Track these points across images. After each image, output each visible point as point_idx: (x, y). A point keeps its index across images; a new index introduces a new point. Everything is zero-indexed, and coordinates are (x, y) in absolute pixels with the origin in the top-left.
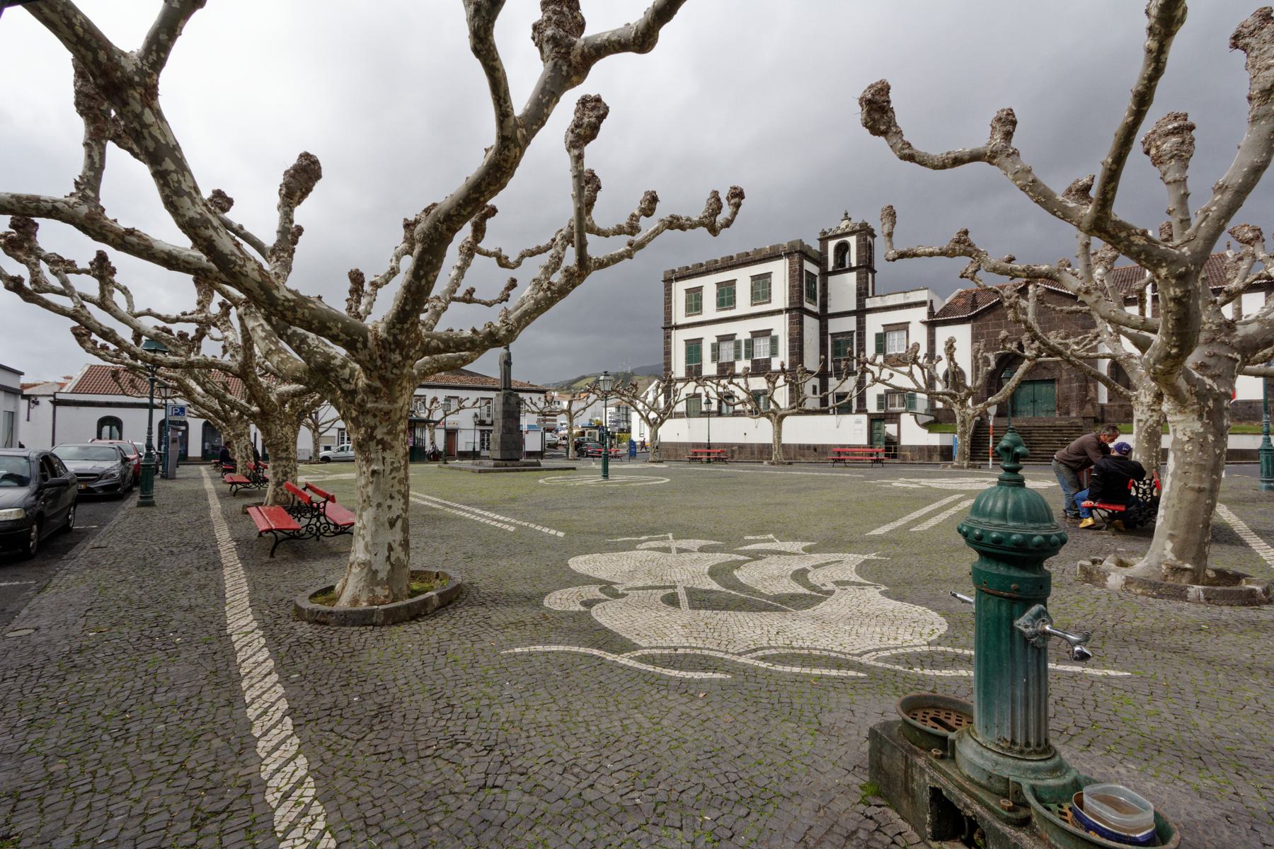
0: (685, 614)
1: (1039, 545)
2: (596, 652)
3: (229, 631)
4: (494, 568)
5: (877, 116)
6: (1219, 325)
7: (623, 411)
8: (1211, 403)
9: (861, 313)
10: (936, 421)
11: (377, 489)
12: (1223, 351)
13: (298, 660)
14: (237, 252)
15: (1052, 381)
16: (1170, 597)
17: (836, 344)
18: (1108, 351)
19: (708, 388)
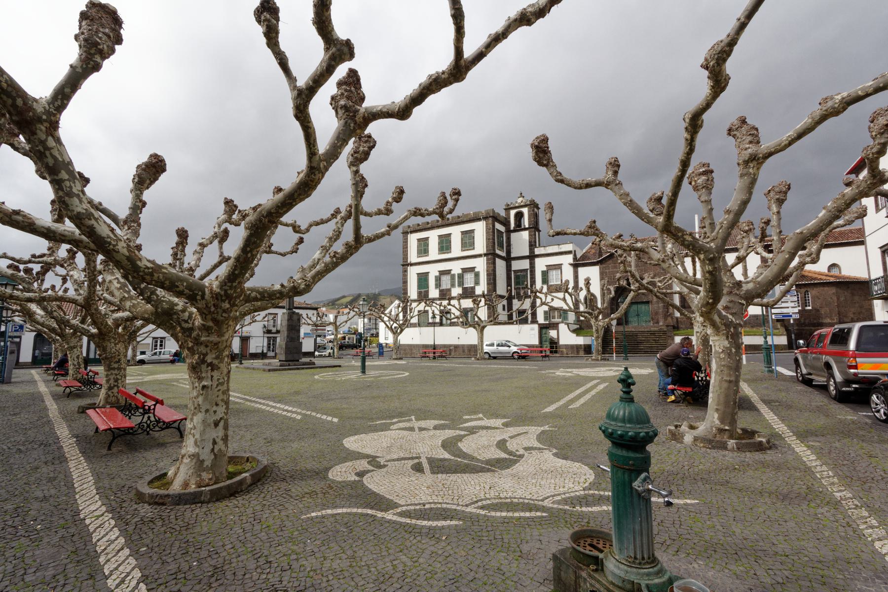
0: (428, 478)
1: (643, 438)
2: (369, 511)
3: (82, 516)
4: (288, 450)
5: (541, 155)
6: (733, 284)
7: (373, 321)
8: (732, 330)
9: (532, 257)
10: (580, 329)
11: (205, 399)
12: (736, 299)
13: (144, 536)
14: (112, 236)
15: (648, 302)
16: (718, 448)
17: (517, 277)
18: (678, 289)
19: (433, 308)
